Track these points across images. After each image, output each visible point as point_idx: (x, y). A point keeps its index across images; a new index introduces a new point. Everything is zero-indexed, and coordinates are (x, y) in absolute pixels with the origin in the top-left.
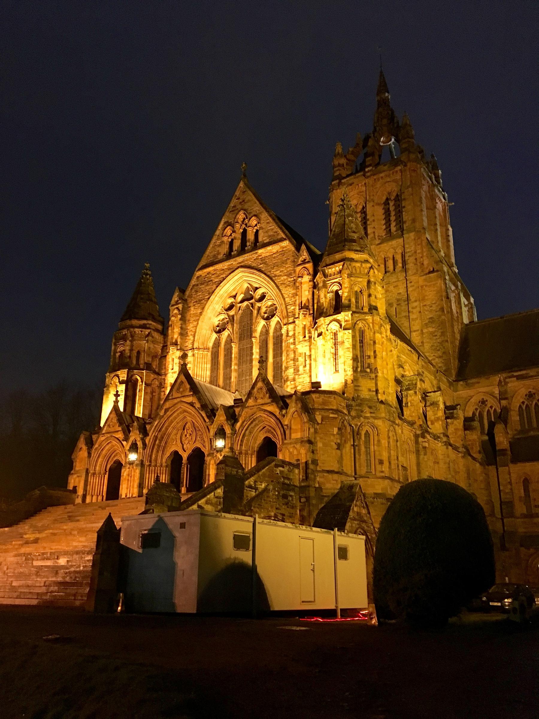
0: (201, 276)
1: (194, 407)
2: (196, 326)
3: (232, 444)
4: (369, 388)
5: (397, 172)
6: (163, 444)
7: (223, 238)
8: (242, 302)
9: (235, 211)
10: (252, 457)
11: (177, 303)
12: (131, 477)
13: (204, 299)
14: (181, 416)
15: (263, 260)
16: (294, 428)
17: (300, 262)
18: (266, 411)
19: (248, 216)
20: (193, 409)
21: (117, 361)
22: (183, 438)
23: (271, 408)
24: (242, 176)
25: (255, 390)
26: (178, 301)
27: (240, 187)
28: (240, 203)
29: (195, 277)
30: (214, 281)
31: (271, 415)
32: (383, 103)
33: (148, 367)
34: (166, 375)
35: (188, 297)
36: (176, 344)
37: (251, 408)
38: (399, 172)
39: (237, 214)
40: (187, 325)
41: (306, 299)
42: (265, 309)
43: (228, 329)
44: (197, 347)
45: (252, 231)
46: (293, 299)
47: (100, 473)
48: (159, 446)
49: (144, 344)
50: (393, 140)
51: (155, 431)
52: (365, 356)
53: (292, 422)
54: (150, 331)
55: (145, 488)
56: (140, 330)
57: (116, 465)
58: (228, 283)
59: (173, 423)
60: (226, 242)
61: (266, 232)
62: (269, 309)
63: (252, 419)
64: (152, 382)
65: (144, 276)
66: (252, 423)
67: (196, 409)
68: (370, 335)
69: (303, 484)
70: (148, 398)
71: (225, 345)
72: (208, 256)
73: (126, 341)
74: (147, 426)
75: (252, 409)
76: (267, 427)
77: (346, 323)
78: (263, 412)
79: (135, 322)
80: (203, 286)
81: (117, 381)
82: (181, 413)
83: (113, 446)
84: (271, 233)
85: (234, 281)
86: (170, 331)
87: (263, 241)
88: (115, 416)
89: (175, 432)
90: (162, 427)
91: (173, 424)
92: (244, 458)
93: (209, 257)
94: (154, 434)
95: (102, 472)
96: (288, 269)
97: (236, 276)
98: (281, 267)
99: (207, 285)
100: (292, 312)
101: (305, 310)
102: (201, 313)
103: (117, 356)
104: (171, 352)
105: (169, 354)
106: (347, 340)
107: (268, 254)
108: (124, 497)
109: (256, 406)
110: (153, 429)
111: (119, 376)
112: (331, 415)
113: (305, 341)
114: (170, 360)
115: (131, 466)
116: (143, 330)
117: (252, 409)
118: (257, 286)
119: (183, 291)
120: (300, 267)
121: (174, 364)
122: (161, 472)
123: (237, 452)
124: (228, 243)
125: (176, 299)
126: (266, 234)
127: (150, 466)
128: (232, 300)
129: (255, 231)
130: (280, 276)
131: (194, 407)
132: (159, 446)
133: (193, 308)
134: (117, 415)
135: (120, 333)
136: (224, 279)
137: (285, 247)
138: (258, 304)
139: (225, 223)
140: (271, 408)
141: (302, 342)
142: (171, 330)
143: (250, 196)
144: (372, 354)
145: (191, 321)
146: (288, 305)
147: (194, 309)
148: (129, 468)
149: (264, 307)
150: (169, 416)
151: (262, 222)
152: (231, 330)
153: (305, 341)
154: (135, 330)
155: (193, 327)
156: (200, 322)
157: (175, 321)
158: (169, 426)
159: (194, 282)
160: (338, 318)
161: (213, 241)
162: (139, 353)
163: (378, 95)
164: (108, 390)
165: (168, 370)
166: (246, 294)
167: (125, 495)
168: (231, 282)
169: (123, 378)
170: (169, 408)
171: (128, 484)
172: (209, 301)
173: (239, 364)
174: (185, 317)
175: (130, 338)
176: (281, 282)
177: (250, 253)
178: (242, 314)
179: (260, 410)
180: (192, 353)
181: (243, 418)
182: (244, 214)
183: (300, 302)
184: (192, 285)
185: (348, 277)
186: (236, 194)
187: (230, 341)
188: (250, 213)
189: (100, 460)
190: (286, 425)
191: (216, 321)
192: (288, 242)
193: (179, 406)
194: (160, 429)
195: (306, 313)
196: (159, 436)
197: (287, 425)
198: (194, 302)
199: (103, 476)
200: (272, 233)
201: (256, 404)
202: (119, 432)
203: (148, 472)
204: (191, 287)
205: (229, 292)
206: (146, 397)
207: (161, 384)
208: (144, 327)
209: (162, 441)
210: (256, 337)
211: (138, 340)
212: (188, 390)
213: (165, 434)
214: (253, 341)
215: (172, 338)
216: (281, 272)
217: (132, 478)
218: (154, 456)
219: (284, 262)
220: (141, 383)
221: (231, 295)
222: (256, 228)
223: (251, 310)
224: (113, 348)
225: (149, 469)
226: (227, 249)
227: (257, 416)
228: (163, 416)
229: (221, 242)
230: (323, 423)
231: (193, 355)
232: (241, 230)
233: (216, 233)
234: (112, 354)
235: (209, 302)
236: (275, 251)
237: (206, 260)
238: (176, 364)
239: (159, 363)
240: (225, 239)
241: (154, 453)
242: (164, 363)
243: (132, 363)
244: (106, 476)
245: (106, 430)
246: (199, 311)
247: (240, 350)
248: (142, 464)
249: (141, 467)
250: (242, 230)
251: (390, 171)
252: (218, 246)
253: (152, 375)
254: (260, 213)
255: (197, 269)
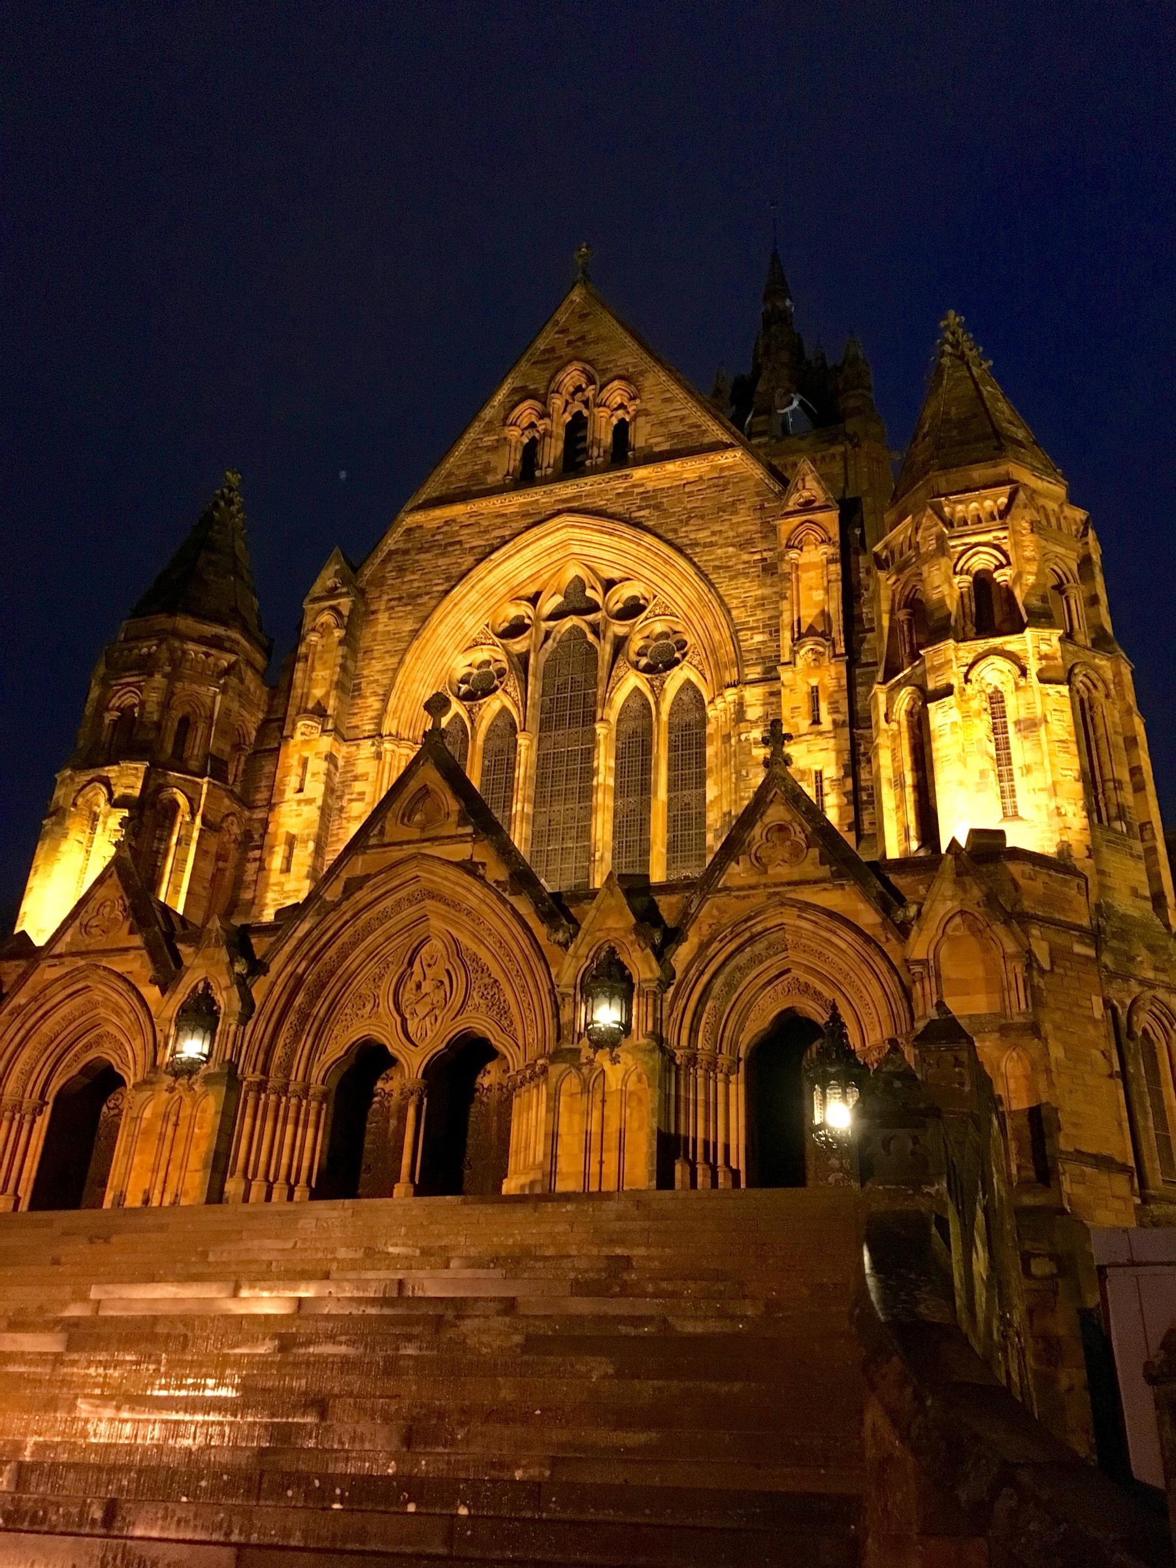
0: (421, 527)
1: (481, 878)
2: (395, 671)
3: (658, 1022)
4: (1133, 884)
5: (833, 456)
6: (320, 1009)
7: (507, 429)
8: (556, 615)
9: (554, 362)
10: (727, 1083)
11: (332, 593)
12: (176, 1125)
13: (427, 594)
14: (409, 913)
15: (651, 499)
16: (954, 976)
17: (791, 505)
18: (808, 906)
19: (597, 376)
20: (477, 888)
21: (105, 736)
22: (407, 995)
23: (831, 899)
24: (580, 275)
25: (757, 831)
26: (336, 588)
27: (572, 302)
28: (570, 342)
29: (401, 530)
30: (467, 546)
31: (833, 925)
32: (776, 319)
33: (217, 769)
34: (271, 806)
35: (369, 583)
36: (320, 712)
37: (742, 893)
38: (838, 458)
39: (558, 370)
40: (360, 664)
41: (815, 611)
42: (641, 643)
43: (505, 691)
44: (394, 732)
45: (608, 422)
46: (758, 612)
47: (17, 1107)
48: (304, 1017)
49: (213, 697)
50: (795, 404)
51: (298, 958)
52: (1104, 781)
53: (944, 951)
54: (236, 662)
55: (232, 1175)
56: (204, 649)
57: (86, 1081)
58: (518, 556)
59: (370, 933)
60: (513, 444)
61: (661, 423)
62: (654, 644)
63: (747, 935)
64: (222, 821)
65: (222, 504)
66: (739, 949)
67: (488, 886)
68: (1113, 716)
69: (1027, 1200)
70: (208, 868)
71: (487, 739)
72: (450, 474)
73: (151, 675)
74: (253, 941)
75: (748, 897)
76: (795, 972)
77: (1044, 662)
78: (795, 911)
79: (185, 623)
80: (428, 556)
81: (102, 799)
82: (411, 900)
83: (95, 1005)
84: (677, 427)
85: (537, 551)
86: (298, 675)
87: (651, 447)
88: (121, 892)
89: (371, 969)
90: (325, 945)
91: (371, 938)
92: (700, 1080)
93: (453, 478)
94: (289, 969)
95: (27, 1105)
96: (741, 530)
97: (548, 539)
98: (716, 520)
99: (443, 555)
100: (758, 650)
101: (820, 639)
102: (415, 634)
103: (107, 721)
104: (298, 737)
105: (292, 742)
106: (1057, 715)
107: (666, 484)
108: (138, 1204)
109: (766, 886)
110: (288, 948)
111: (112, 782)
112: (1078, 949)
113: (821, 733)
114: (294, 761)
115: (183, 1081)
116: (213, 651)
117: (748, 897)
118: (615, 574)
119: (355, 568)
120: (795, 520)
121: (308, 776)
122: (302, 1117)
123: (679, 1053)
124: (520, 448)
125: (330, 583)
126: (662, 430)
127: (261, 1087)
128: (524, 609)
129: (615, 421)
130: (712, 544)
131: (481, 878)
132: (304, 1017)
133: (386, 615)
134: (126, 889)
135: (130, 650)
136: (506, 542)
137: (729, 468)
138: (618, 628)
139: (514, 391)
140: (831, 899)
141: (808, 737)
142: (305, 671)
143: (607, 325)
144: (1125, 776)
145: (376, 654)
146: (741, 630)
147: (390, 618)
148: (171, 1090)
149: (639, 636)
150: (360, 906)
151: (645, 396)
152: (517, 694)
153: (821, 733)
154: (185, 646)
155: (382, 672)
156: (408, 658)
157: (319, 648)
158: (354, 944)
159: (393, 541)
160: (1008, 648)
161: (471, 435)
162: (185, 724)
163: (766, 298)
164: (60, 823)
165: (282, 792)
166: (572, 598)
167: (140, 1197)
168: (528, 553)
169: (129, 791)
170: (368, 877)
171: (159, 1154)
172: (448, 598)
173: (539, 800)
174: (357, 640)
175: (168, 669)
176: (717, 563)
177: (607, 476)
178: (554, 652)
179: (782, 904)
180: (374, 749)
181: (705, 927)
182: (584, 371)
183: (796, 618)
184: (386, 549)
185: (1032, 531)
186: (557, 316)
187: (506, 728)
188: (603, 372)
189: (26, 1054)
190: (918, 962)
191: (461, 665)
192: (739, 454)
193: (409, 871)
194: (318, 953)
195: (821, 649)
196: (310, 978)
197: (924, 963)
198: (391, 600)
199: (28, 1118)
200: (680, 429)
201: (763, 880)
202: (132, 954)
203: (249, 1111)
204: (381, 556)
205: (516, 583)
206: (201, 864)
207: (248, 834)
208: (216, 643)
209: (318, 997)
210: (607, 721)
211: (193, 682)
212: (454, 818)
213: (333, 973)
214: (598, 731)
215: (306, 696)
216: (713, 534)
217: (182, 1130)
218: (279, 1052)
219: (732, 507)
220: (188, 819)
221: (522, 593)
222: (620, 413)
223: (591, 645)
224: (95, 692)
225: (258, 1099)
226: (517, 463)
227: (770, 924)
228: (337, 905)
229: (497, 441)
230: (1057, 970)
231: (379, 756)
232: (568, 418)
233: (482, 415)
234: (89, 710)
235: (447, 603)
236: (690, 476)
237: (443, 484)
238: (314, 775)
239: (244, 771)
240: (514, 433)
241: (281, 1042)
242: (268, 769)
243: (162, 749)
244: (39, 1119)
245: (71, 943)
246: (409, 626)
247: (542, 760)
248: (231, 1077)
249: (229, 1088)
250: (570, 419)
251: (816, 452)
252: (488, 451)
253: (226, 801)
254: (642, 373)
255: (409, 506)
